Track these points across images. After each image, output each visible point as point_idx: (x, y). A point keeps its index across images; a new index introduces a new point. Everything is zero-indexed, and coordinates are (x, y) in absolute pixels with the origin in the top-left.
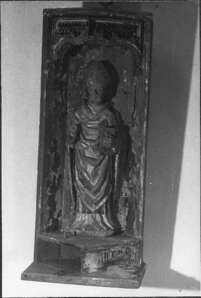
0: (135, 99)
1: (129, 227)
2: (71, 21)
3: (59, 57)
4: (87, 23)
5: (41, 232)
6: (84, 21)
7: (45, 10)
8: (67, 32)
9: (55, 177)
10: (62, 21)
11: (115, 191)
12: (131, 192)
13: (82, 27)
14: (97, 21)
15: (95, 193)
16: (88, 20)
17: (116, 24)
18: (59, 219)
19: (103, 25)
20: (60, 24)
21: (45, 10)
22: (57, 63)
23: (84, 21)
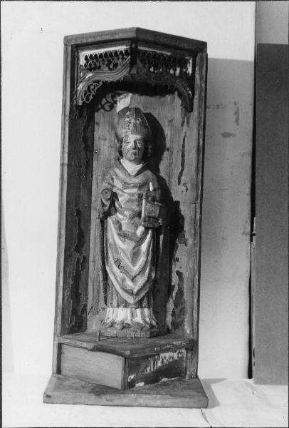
0: (183, 156)
1: (177, 325)
2: (102, 51)
3: (85, 100)
4: (126, 51)
5: (62, 334)
6: (122, 48)
7: (74, 47)
8: (96, 66)
9: (78, 260)
10: (88, 53)
11: (158, 276)
12: (104, 104)
13: (121, 57)
14: (140, 48)
15: (133, 279)
16: (128, 47)
17: (163, 55)
18: (84, 316)
19: (162, 58)
20: (86, 56)
21: (74, 47)
22: (81, 108)
23: (122, 48)
